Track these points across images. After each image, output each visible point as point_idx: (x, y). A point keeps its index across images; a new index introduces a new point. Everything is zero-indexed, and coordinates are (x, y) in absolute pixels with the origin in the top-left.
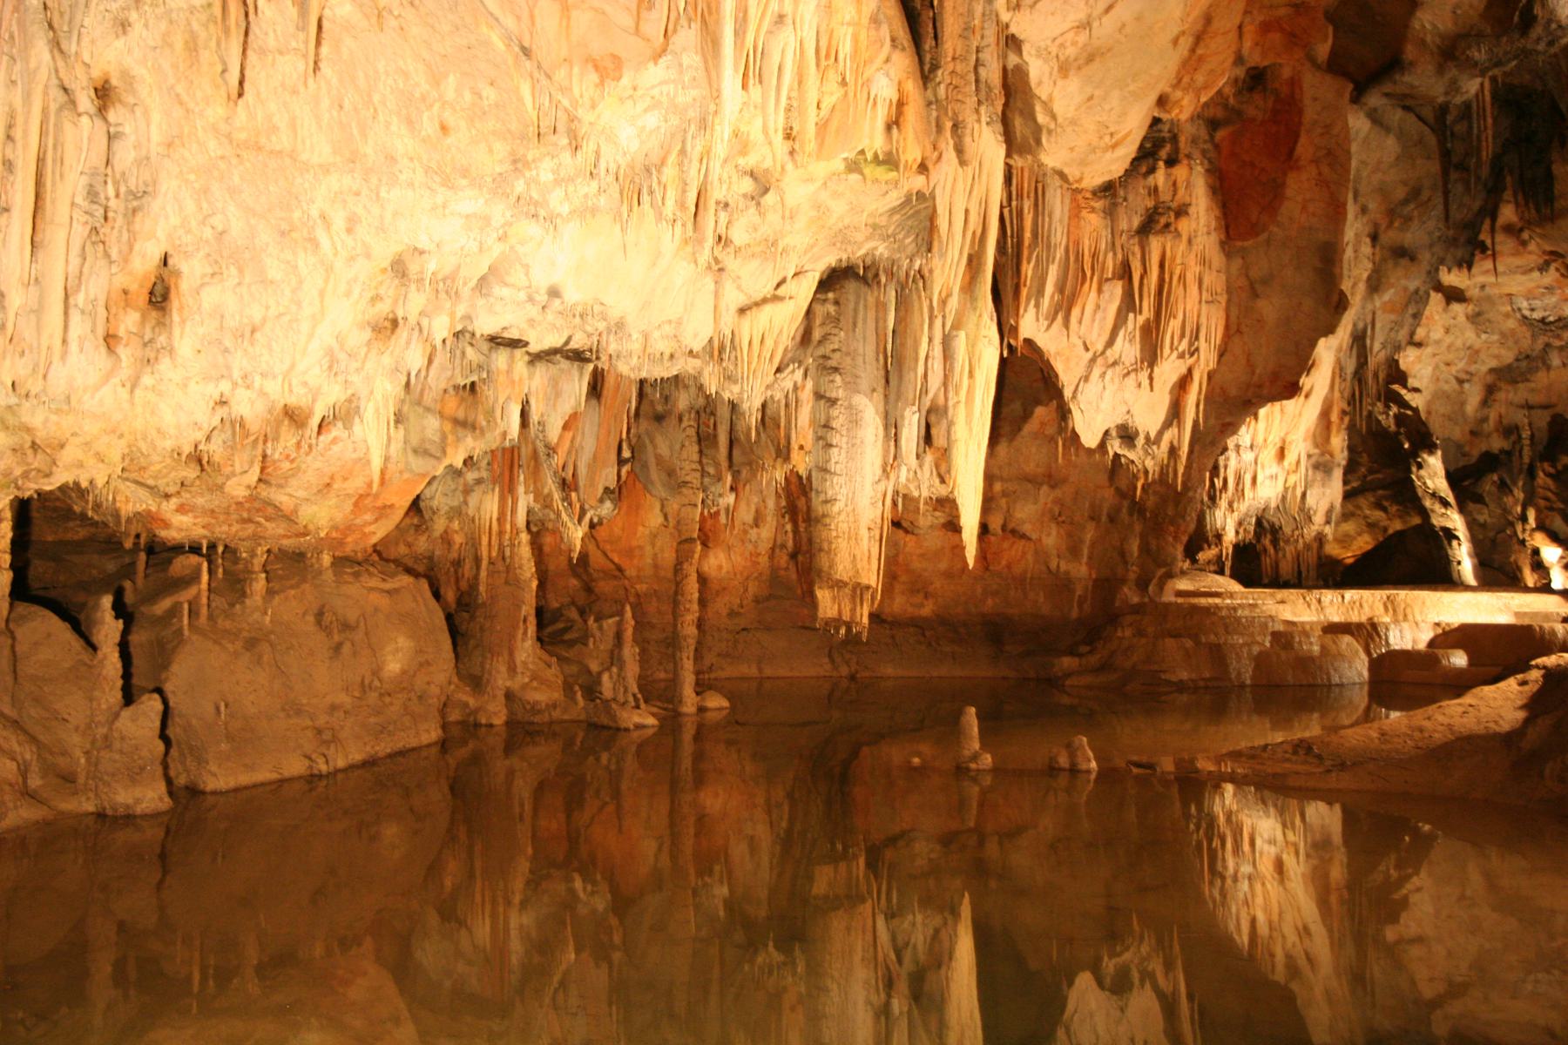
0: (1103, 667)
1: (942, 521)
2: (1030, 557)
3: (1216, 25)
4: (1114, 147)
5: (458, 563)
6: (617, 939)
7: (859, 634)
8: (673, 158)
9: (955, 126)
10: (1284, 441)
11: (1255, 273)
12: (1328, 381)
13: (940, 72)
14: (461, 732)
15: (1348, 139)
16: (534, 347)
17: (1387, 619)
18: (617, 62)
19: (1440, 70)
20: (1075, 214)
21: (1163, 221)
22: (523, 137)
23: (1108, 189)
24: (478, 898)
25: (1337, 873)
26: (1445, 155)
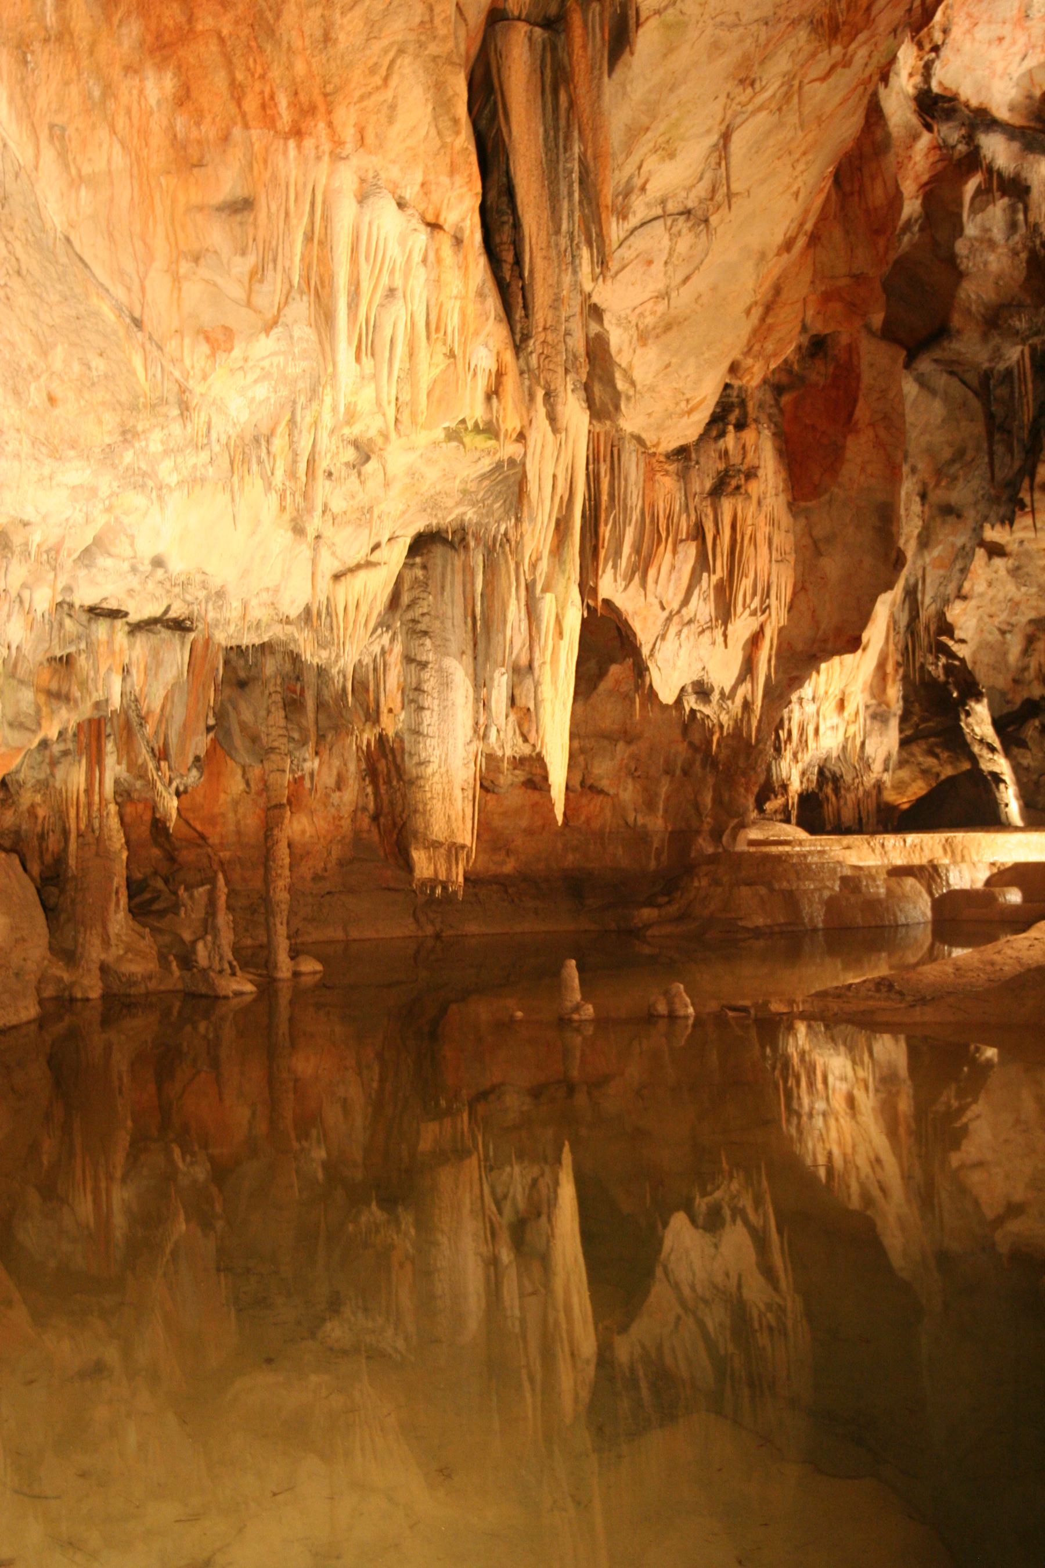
0: (682, 918)
1: (522, 779)
2: (608, 812)
3: (784, 296)
4: (690, 412)
5: (42, 837)
6: (218, 1209)
7: (455, 893)
8: (282, 428)
9: (548, 395)
10: (843, 693)
11: (818, 532)
12: (883, 635)
13: (531, 342)
14: (61, 1004)
16: (134, 617)
17: (946, 861)
18: (228, 333)
19: (985, 338)
20: (650, 476)
21: (734, 483)
23: (682, 453)
24: (79, 1173)
25: (905, 1105)
26: (990, 417)
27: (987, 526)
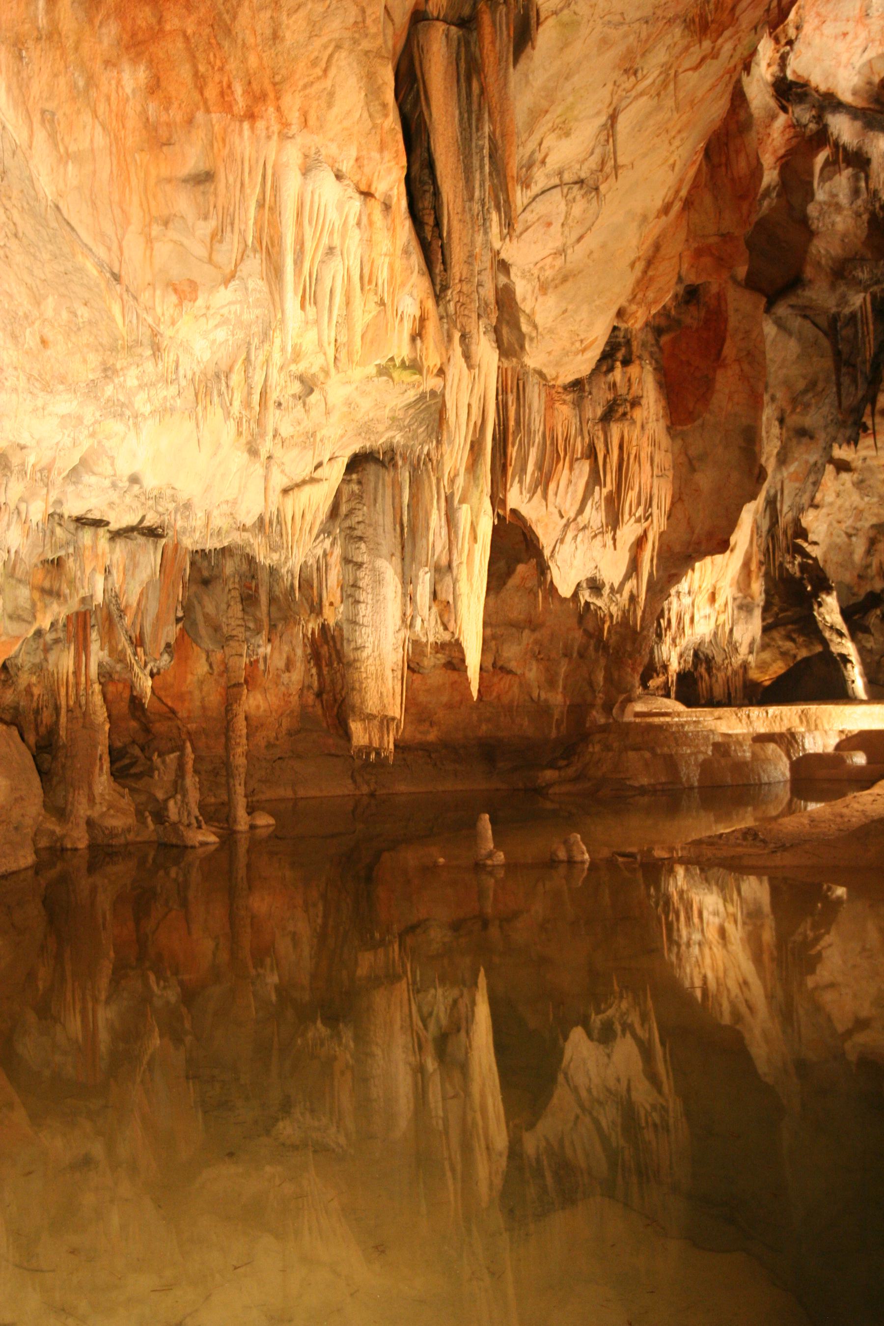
0: (577, 778)
1: (443, 661)
2: (516, 689)
3: (663, 252)
4: (584, 351)
5: (37, 712)
6: (187, 1025)
7: (387, 758)
9: (463, 337)
10: (715, 588)
11: (692, 452)
12: (748, 538)
14: (54, 853)
15: (763, 341)
16: (114, 526)
17: (802, 729)
18: (193, 285)
19: (833, 287)
21: (621, 410)
22: (113, 349)
23: (577, 385)
25: (768, 936)
26: (837, 354)
27: (836, 446)
